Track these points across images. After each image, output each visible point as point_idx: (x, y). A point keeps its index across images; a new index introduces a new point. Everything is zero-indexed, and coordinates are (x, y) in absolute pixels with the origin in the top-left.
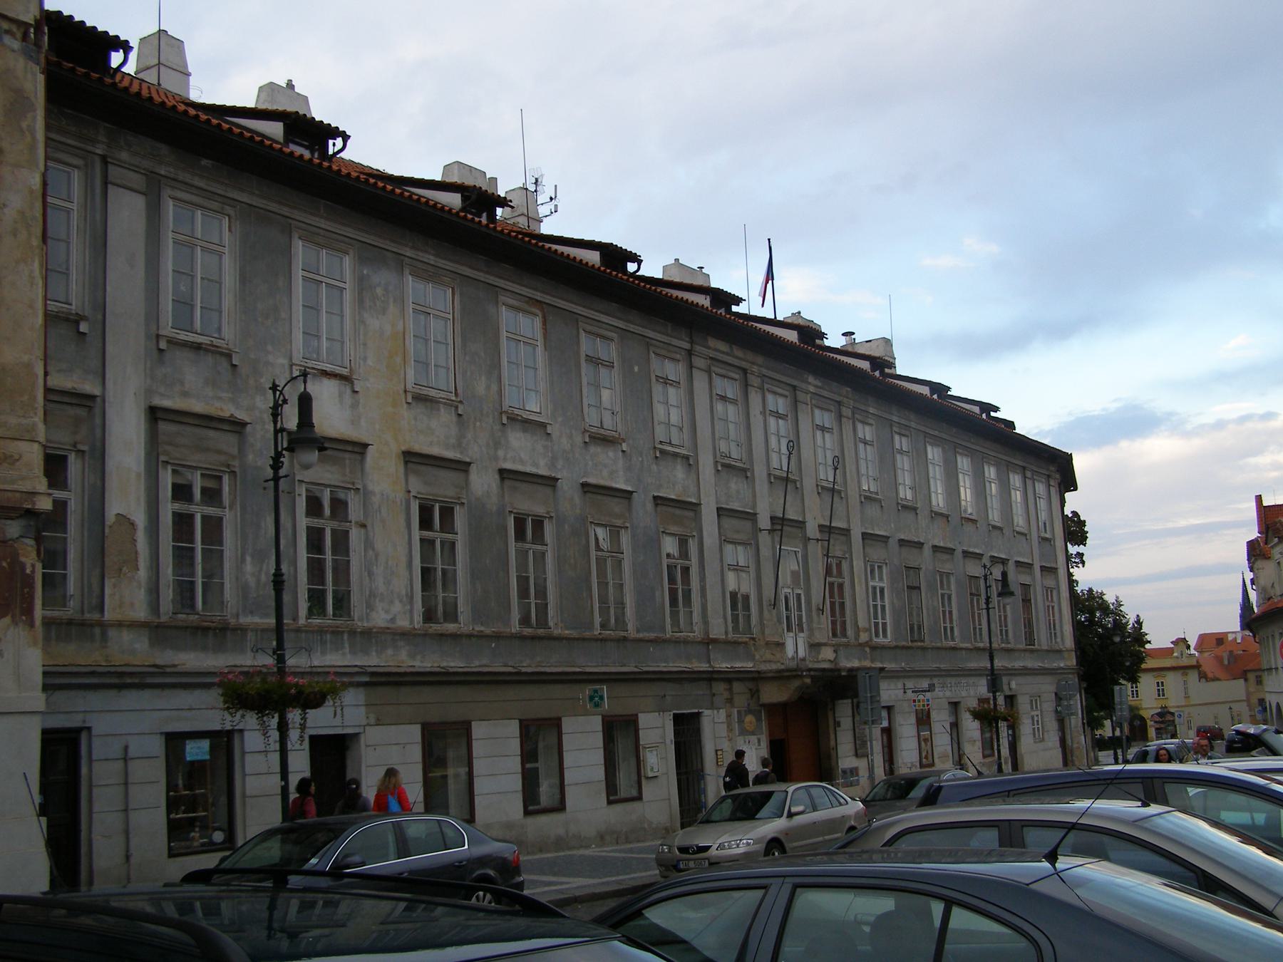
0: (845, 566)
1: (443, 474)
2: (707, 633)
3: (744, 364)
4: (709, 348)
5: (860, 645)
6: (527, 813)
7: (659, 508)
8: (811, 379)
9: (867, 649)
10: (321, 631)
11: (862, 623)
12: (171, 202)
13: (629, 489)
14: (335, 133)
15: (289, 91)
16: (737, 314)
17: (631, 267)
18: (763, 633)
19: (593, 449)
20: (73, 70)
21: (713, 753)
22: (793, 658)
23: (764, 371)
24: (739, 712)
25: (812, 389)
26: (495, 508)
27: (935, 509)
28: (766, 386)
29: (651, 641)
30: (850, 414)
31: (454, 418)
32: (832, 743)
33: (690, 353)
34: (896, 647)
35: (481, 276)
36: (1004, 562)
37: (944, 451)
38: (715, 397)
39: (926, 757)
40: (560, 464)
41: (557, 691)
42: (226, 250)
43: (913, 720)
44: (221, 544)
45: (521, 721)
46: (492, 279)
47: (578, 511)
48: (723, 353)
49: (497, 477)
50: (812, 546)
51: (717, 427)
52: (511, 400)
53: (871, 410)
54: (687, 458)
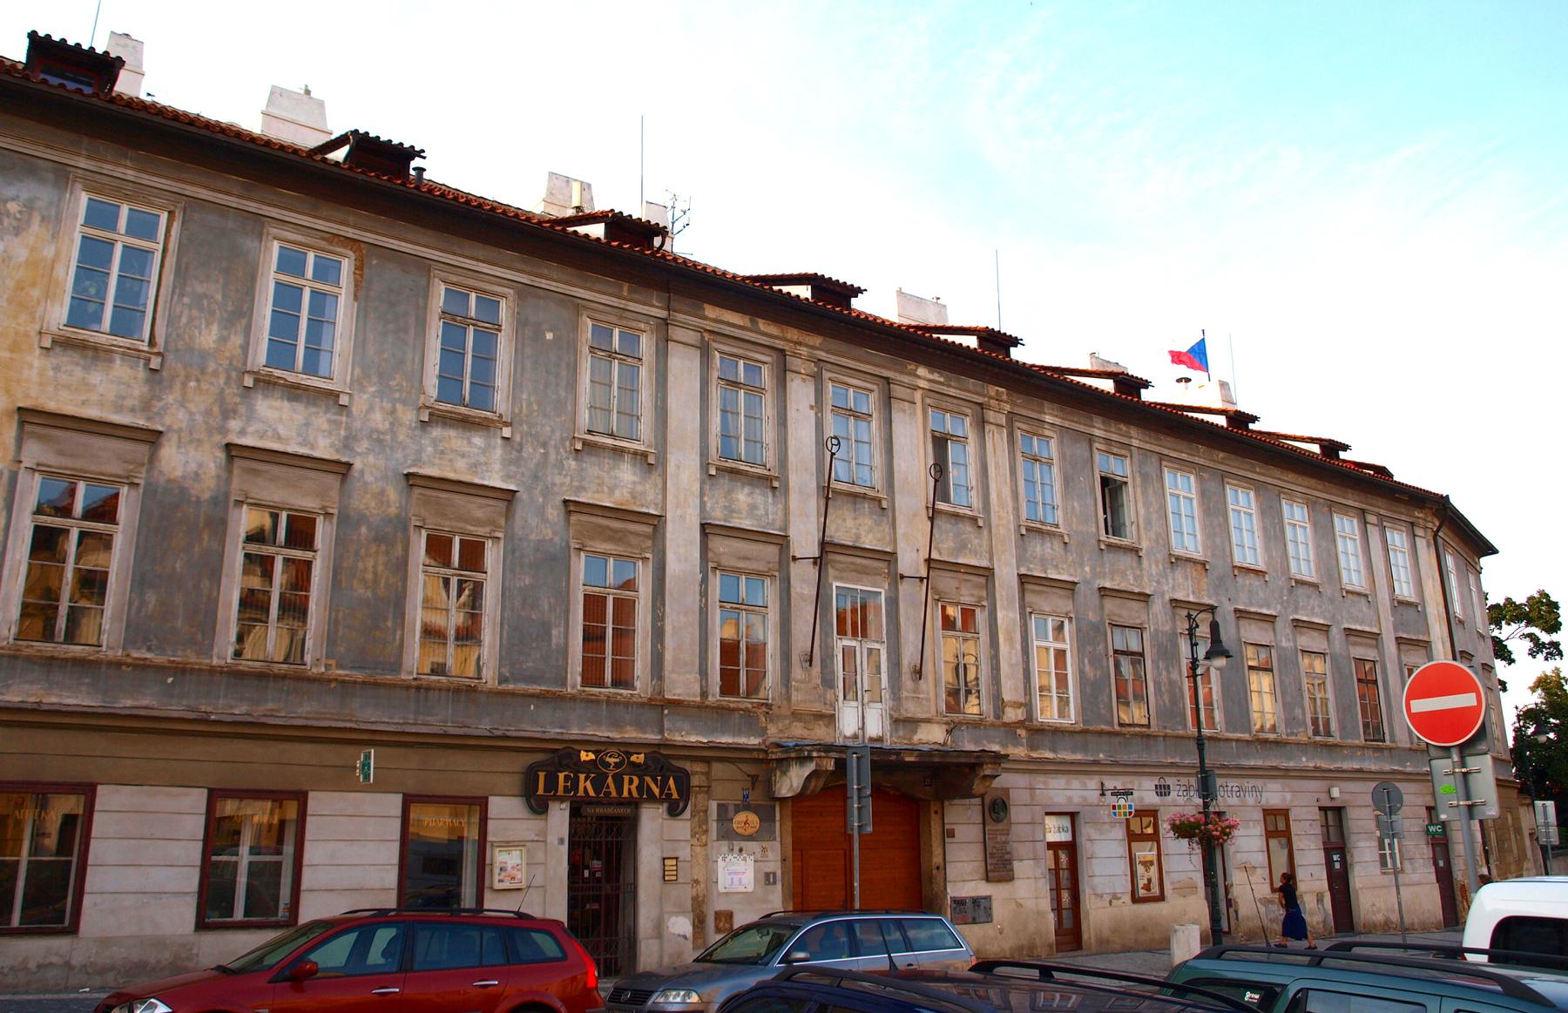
0: (981, 617)
1: (97, 442)
2: (661, 692)
3: (779, 344)
4: (706, 318)
5: (1005, 725)
6: (202, 925)
7: (574, 518)
8: (922, 371)
9: (1022, 732)
10: (593, 701)
11: (1007, 696)
12: (830, 385)
13: (513, 487)
14: (412, 153)
15: (305, 98)
16: (1344, 461)
17: (657, 241)
18: (789, 699)
19: (437, 432)
20: (62, 86)
21: (657, 865)
22: (855, 736)
23: (822, 355)
24: (722, 808)
25: (922, 384)
26: (207, 495)
27: (1349, 588)
28: (826, 375)
29: (532, 696)
30: (1003, 421)
31: (142, 374)
32: (937, 860)
33: (666, 323)
34: (1084, 732)
35: (232, 201)
36: (1212, 609)
37: (1200, 480)
38: (1019, 459)
39: (1147, 887)
40: (363, 446)
41: (303, 753)
43: (1119, 833)
44: (307, 590)
45: (405, 795)
46: (252, 206)
47: (393, 510)
48: (770, 336)
49: (221, 455)
50: (904, 588)
51: (878, 460)
52: (1238, 559)
53: (1048, 418)
54: (974, 519)
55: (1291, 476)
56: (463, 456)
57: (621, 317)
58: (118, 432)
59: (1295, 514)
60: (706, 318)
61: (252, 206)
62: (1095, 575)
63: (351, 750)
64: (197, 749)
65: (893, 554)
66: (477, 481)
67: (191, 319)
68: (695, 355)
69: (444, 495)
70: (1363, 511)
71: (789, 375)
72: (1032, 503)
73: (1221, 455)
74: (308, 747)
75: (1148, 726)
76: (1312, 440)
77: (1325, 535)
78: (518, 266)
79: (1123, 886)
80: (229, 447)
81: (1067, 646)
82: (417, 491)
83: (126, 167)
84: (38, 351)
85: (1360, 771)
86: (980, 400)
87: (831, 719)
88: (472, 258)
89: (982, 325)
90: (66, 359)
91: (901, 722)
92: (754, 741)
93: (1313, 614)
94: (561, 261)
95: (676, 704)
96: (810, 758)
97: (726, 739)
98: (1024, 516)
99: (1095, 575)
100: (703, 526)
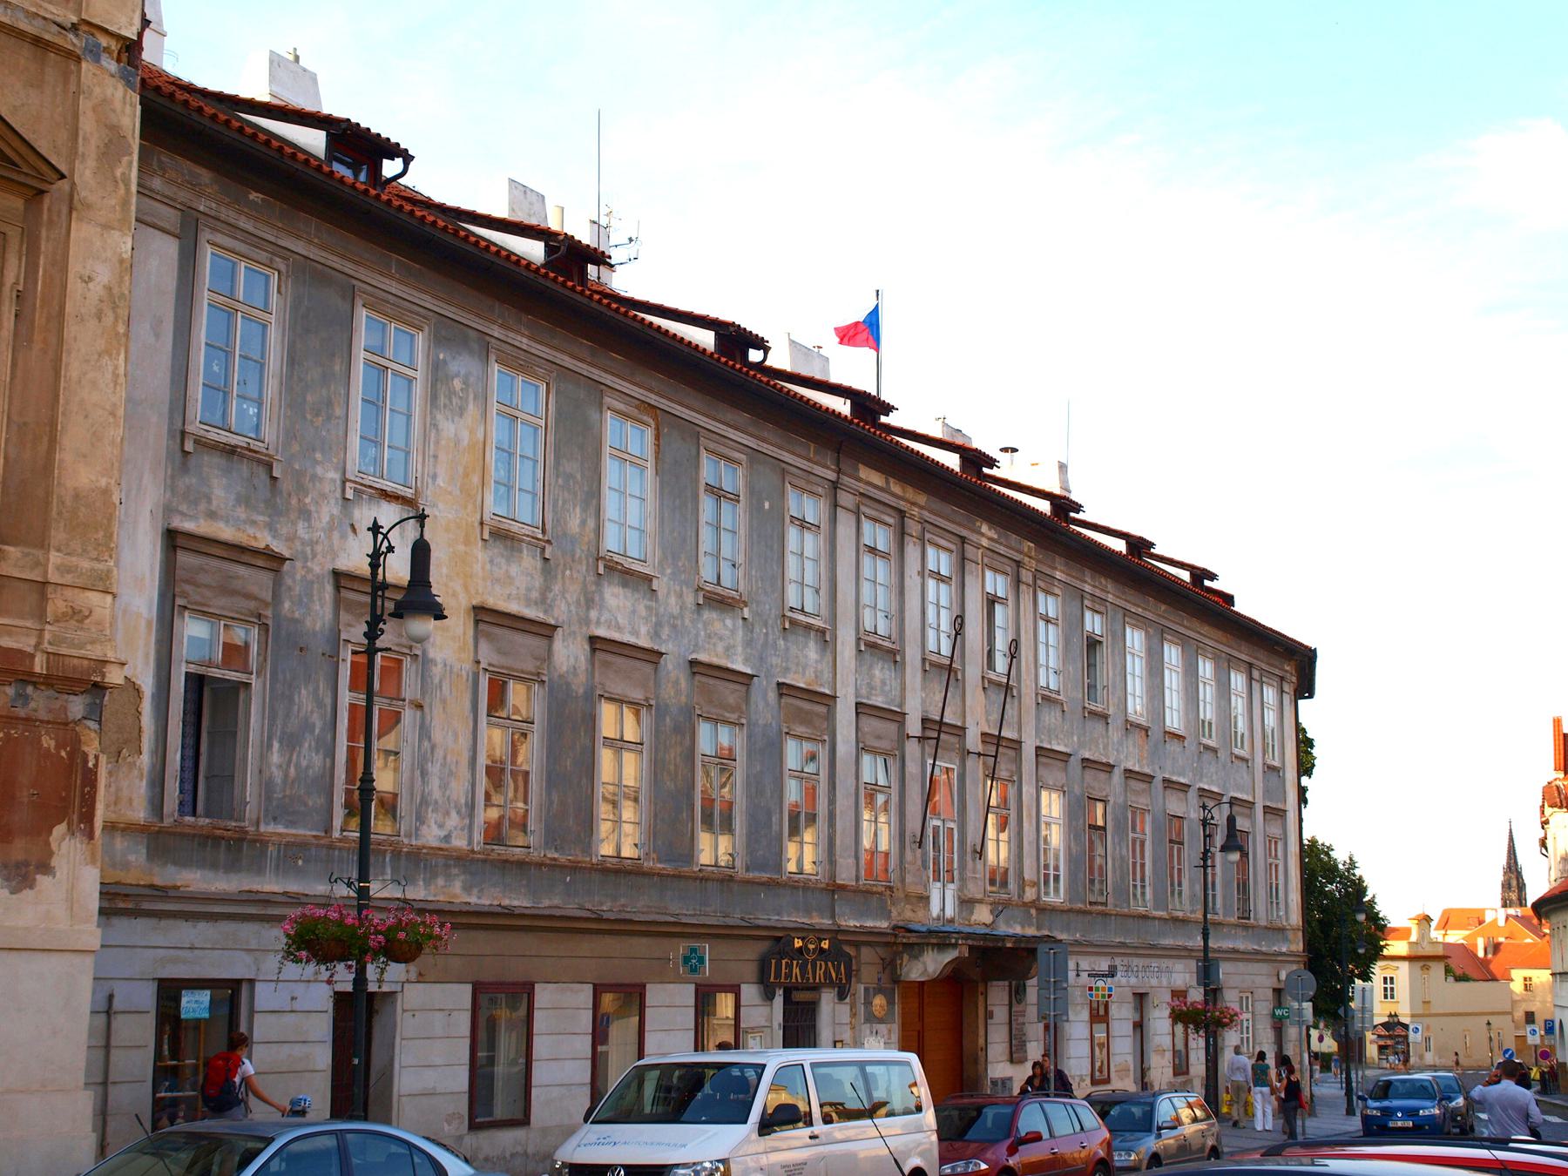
2: (833, 876)
3: (902, 505)
4: (859, 480)
7: (785, 700)
8: (985, 528)
19: (707, 615)
25: (985, 542)
29: (762, 884)
31: (539, 564)
32: (981, 1041)
33: (835, 486)
41: (641, 946)
42: (273, 319)
46: (596, 374)
50: (971, 762)
53: (1058, 575)
55: (1206, 629)
56: (721, 639)
57: (809, 482)
58: (534, 629)
59: (626, 440)
60: (859, 480)
61: (596, 374)
62: (1081, 745)
63: (666, 942)
64: (586, 946)
65: (963, 729)
66: (730, 666)
67: (564, 502)
68: (853, 518)
69: (712, 681)
70: (1251, 665)
71: (907, 538)
72: (219, 389)
73: (1163, 607)
74: (644, 940)
75: (1105, 904)
76: (1182, 565)
77: (677, 489)
78: (751, 429)
79: (1086, 1071)
80: (593, 640)
81: (1131, 835)
82: (698, 677)
83: (523, 335)
84: (480, 543)
85: (1257, 952)
86: (1018, 557)
87: (925, 900)
88: (687, 407)
89: (1136, 531)
90: (497, 549)
91: (966, 903)
92: (884, 925)
93: (1212, 782)
94: (776, 423)
95: (843, 888)
96: (955, 946)
97: (869, 924)
98: (196, 410)
99: (1081, 745)
100: (858, 704)
